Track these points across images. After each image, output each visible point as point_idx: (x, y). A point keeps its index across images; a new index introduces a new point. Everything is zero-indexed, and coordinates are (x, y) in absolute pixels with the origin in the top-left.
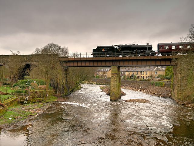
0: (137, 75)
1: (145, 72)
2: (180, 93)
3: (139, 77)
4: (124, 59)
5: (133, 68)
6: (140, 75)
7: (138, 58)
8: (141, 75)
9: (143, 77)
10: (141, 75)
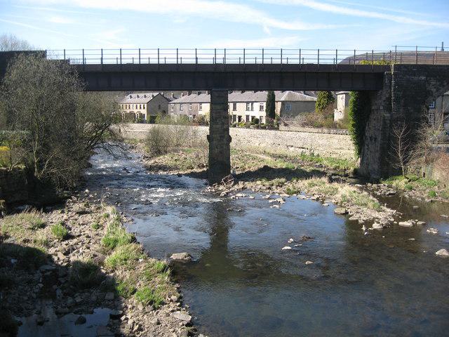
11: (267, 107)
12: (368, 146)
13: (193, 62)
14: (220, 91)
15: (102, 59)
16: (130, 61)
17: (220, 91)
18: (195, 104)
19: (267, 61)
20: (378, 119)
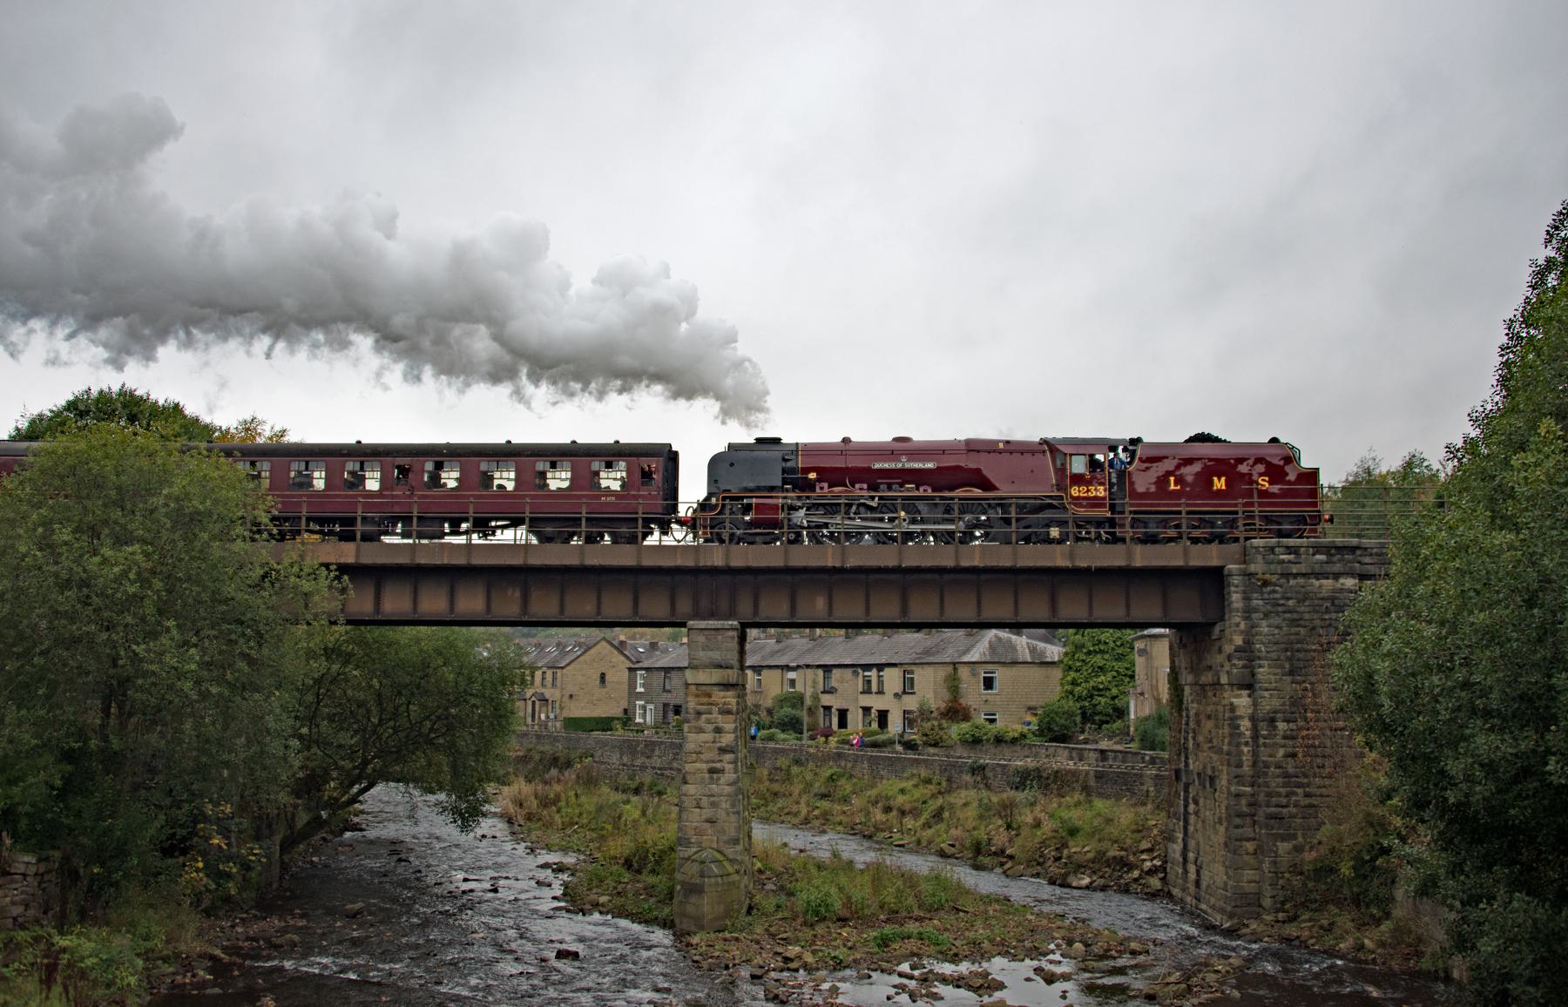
0: (826, 700)
1: (893, 678)
2: (1250, 846)
3: (843, 714)
4: (1030, 563)
5: (788, 637)
6: (847, 693)
7: (913, 556)
8: (866, 701)
9: (883, 716)
10: (866, 701)
12: (1196, 802)
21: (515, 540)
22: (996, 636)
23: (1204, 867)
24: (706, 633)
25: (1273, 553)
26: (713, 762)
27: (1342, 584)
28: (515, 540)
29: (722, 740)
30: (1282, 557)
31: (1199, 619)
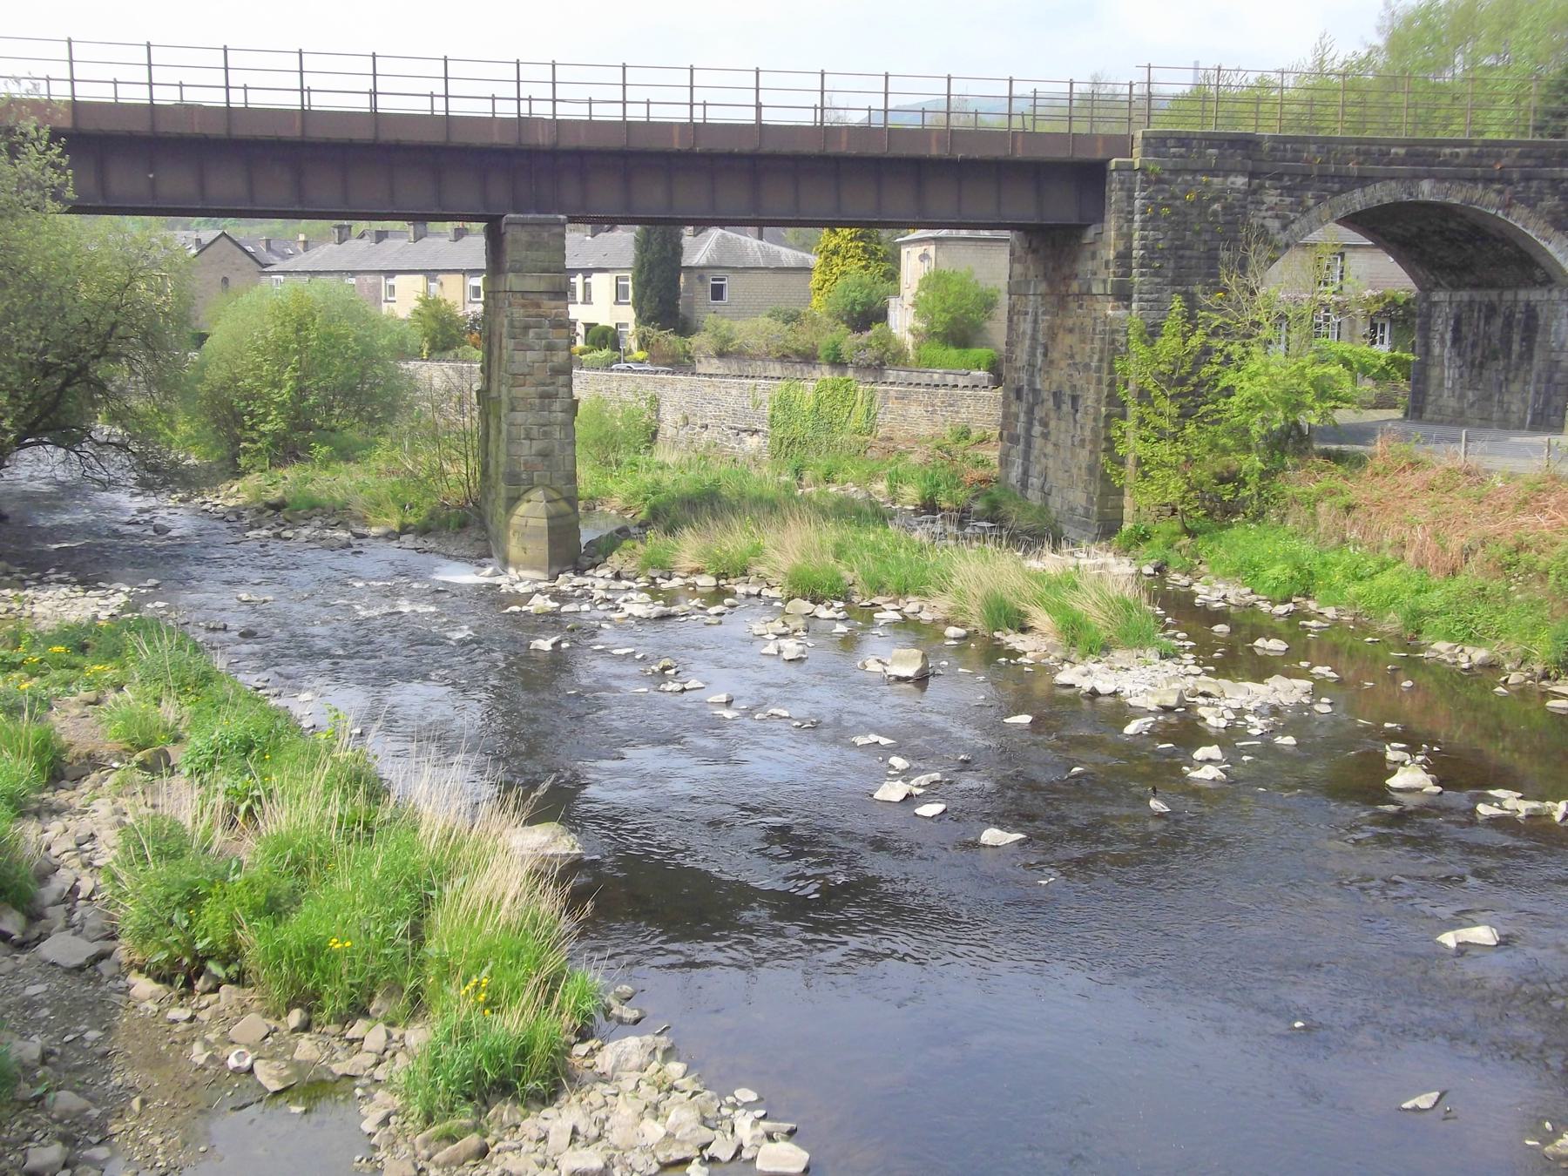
11: (637, 285)
12: (1045, 424)
13: (747, 116)
14: (541, 224)
15: (759, 107)
16: (481, 109)
17: (541, 224)
18: (370, 279)
19: (166, 96)
20: (1082, 330)
21: (303, 105)
22: (723, 236)
23: (1053, 493)
24: (529, 229)
25: (1165, 146)
26: (544, 384)
27: (1232, 183)
28: (303, 105)
29: (555, 359)
30: (1173, 150)
31: (1074, 221)
